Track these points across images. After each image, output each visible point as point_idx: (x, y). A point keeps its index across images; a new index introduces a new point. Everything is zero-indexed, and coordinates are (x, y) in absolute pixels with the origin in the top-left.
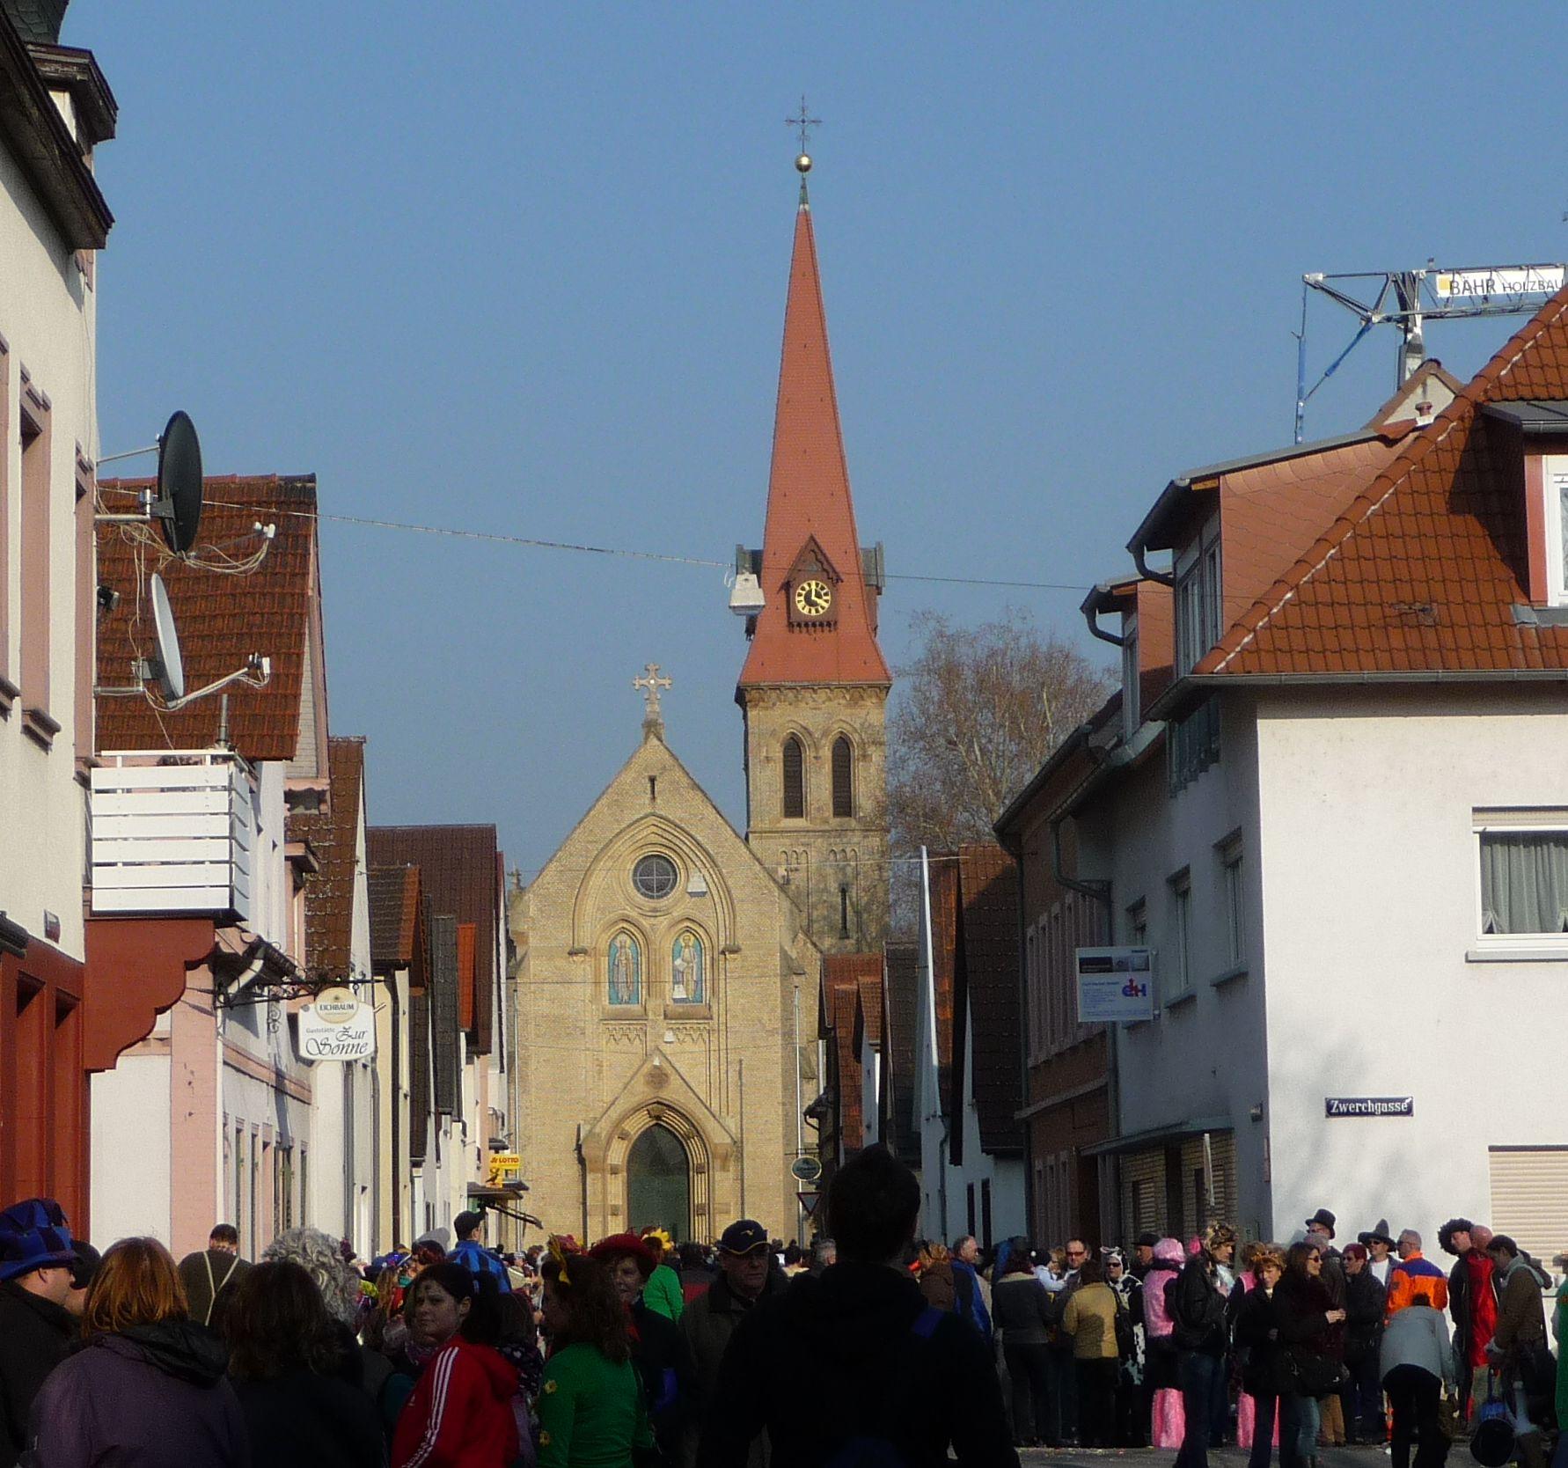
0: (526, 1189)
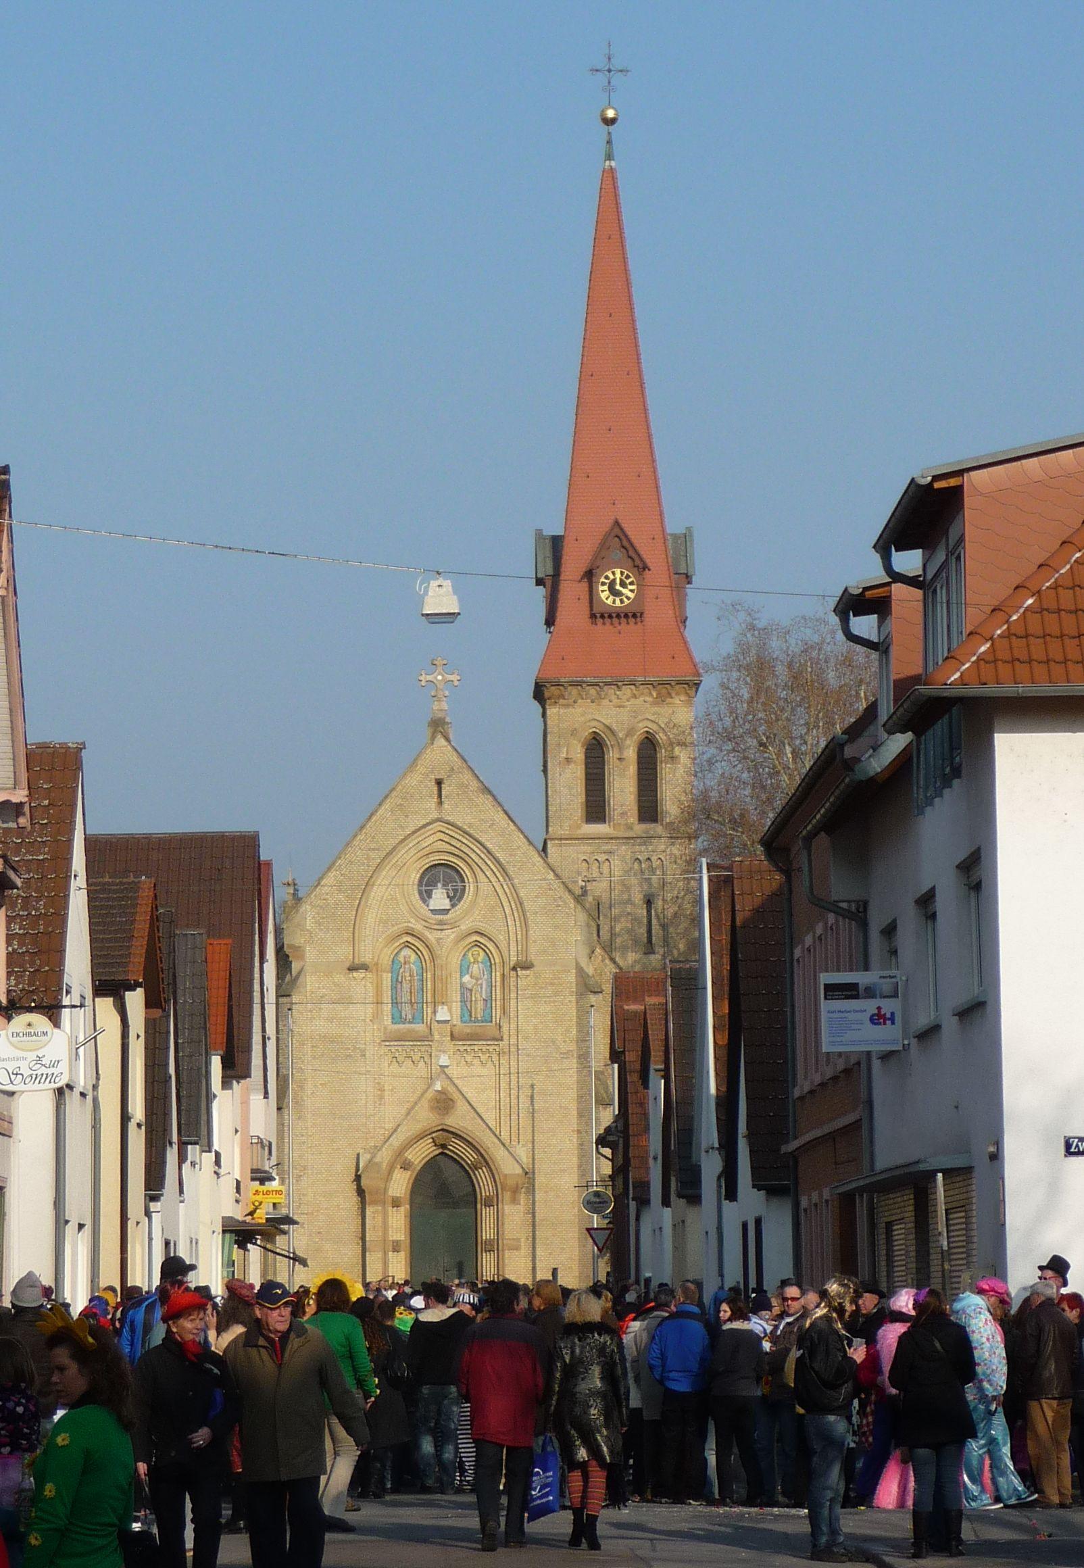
0: (295, 1223)
